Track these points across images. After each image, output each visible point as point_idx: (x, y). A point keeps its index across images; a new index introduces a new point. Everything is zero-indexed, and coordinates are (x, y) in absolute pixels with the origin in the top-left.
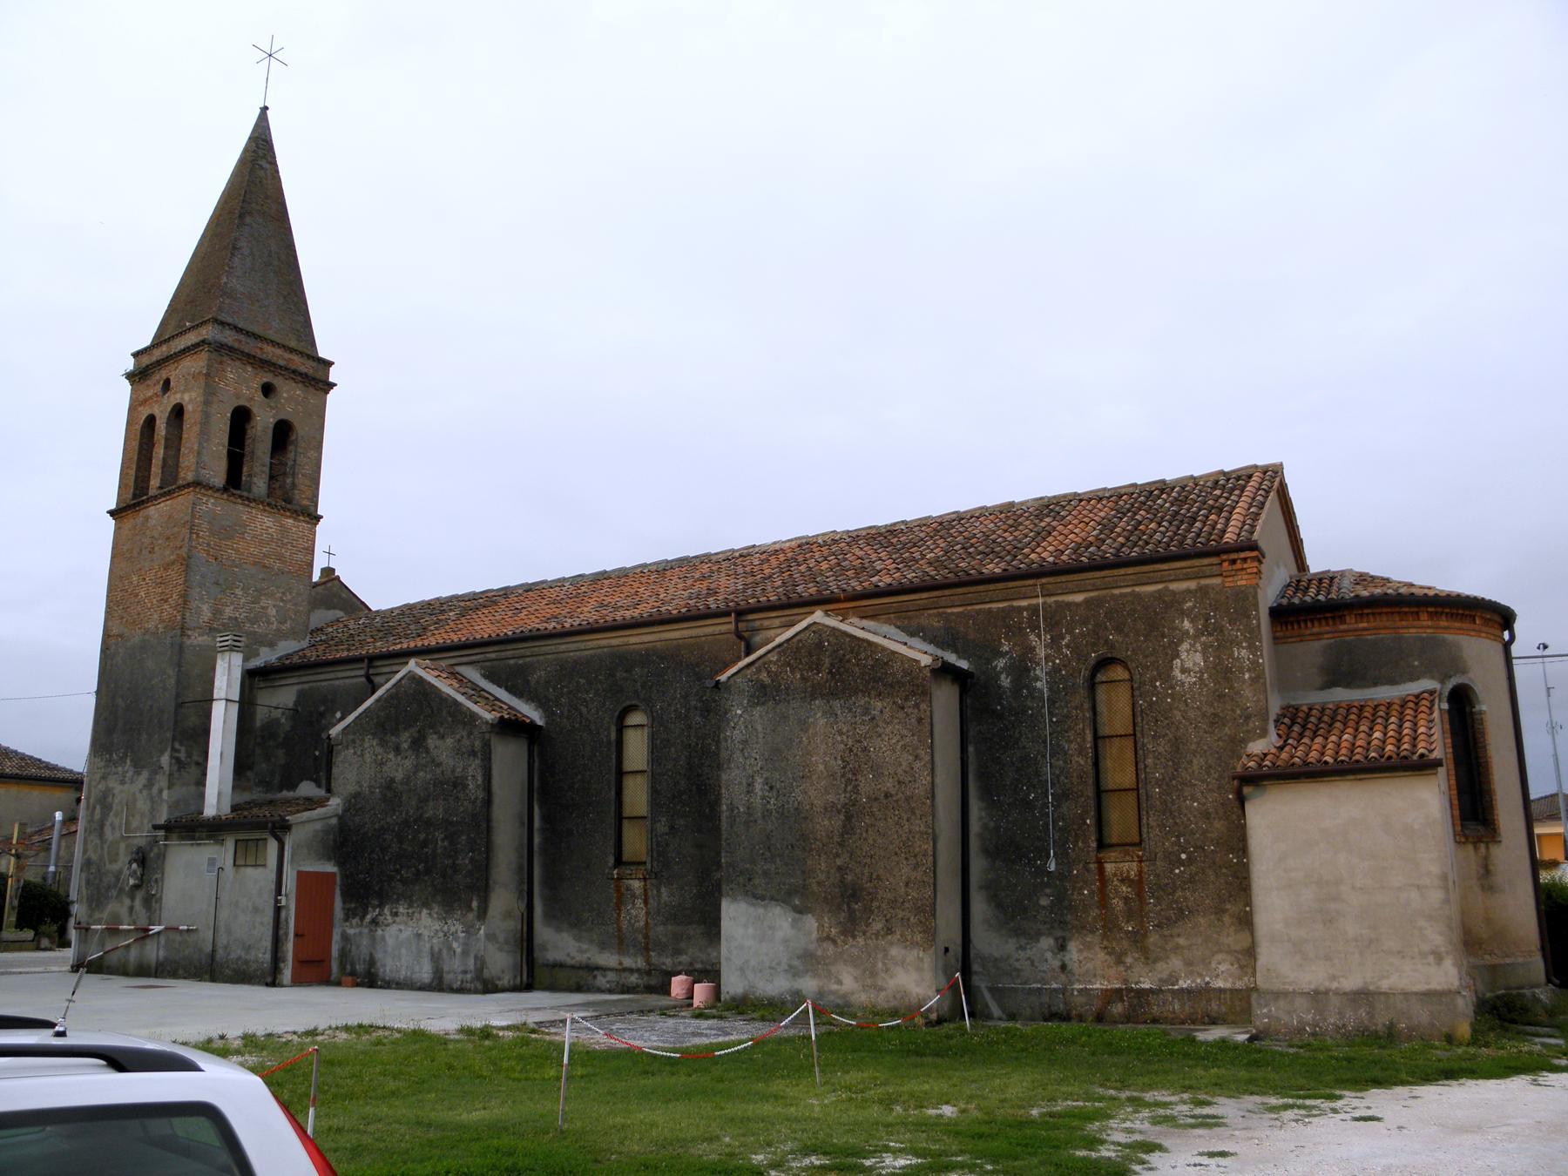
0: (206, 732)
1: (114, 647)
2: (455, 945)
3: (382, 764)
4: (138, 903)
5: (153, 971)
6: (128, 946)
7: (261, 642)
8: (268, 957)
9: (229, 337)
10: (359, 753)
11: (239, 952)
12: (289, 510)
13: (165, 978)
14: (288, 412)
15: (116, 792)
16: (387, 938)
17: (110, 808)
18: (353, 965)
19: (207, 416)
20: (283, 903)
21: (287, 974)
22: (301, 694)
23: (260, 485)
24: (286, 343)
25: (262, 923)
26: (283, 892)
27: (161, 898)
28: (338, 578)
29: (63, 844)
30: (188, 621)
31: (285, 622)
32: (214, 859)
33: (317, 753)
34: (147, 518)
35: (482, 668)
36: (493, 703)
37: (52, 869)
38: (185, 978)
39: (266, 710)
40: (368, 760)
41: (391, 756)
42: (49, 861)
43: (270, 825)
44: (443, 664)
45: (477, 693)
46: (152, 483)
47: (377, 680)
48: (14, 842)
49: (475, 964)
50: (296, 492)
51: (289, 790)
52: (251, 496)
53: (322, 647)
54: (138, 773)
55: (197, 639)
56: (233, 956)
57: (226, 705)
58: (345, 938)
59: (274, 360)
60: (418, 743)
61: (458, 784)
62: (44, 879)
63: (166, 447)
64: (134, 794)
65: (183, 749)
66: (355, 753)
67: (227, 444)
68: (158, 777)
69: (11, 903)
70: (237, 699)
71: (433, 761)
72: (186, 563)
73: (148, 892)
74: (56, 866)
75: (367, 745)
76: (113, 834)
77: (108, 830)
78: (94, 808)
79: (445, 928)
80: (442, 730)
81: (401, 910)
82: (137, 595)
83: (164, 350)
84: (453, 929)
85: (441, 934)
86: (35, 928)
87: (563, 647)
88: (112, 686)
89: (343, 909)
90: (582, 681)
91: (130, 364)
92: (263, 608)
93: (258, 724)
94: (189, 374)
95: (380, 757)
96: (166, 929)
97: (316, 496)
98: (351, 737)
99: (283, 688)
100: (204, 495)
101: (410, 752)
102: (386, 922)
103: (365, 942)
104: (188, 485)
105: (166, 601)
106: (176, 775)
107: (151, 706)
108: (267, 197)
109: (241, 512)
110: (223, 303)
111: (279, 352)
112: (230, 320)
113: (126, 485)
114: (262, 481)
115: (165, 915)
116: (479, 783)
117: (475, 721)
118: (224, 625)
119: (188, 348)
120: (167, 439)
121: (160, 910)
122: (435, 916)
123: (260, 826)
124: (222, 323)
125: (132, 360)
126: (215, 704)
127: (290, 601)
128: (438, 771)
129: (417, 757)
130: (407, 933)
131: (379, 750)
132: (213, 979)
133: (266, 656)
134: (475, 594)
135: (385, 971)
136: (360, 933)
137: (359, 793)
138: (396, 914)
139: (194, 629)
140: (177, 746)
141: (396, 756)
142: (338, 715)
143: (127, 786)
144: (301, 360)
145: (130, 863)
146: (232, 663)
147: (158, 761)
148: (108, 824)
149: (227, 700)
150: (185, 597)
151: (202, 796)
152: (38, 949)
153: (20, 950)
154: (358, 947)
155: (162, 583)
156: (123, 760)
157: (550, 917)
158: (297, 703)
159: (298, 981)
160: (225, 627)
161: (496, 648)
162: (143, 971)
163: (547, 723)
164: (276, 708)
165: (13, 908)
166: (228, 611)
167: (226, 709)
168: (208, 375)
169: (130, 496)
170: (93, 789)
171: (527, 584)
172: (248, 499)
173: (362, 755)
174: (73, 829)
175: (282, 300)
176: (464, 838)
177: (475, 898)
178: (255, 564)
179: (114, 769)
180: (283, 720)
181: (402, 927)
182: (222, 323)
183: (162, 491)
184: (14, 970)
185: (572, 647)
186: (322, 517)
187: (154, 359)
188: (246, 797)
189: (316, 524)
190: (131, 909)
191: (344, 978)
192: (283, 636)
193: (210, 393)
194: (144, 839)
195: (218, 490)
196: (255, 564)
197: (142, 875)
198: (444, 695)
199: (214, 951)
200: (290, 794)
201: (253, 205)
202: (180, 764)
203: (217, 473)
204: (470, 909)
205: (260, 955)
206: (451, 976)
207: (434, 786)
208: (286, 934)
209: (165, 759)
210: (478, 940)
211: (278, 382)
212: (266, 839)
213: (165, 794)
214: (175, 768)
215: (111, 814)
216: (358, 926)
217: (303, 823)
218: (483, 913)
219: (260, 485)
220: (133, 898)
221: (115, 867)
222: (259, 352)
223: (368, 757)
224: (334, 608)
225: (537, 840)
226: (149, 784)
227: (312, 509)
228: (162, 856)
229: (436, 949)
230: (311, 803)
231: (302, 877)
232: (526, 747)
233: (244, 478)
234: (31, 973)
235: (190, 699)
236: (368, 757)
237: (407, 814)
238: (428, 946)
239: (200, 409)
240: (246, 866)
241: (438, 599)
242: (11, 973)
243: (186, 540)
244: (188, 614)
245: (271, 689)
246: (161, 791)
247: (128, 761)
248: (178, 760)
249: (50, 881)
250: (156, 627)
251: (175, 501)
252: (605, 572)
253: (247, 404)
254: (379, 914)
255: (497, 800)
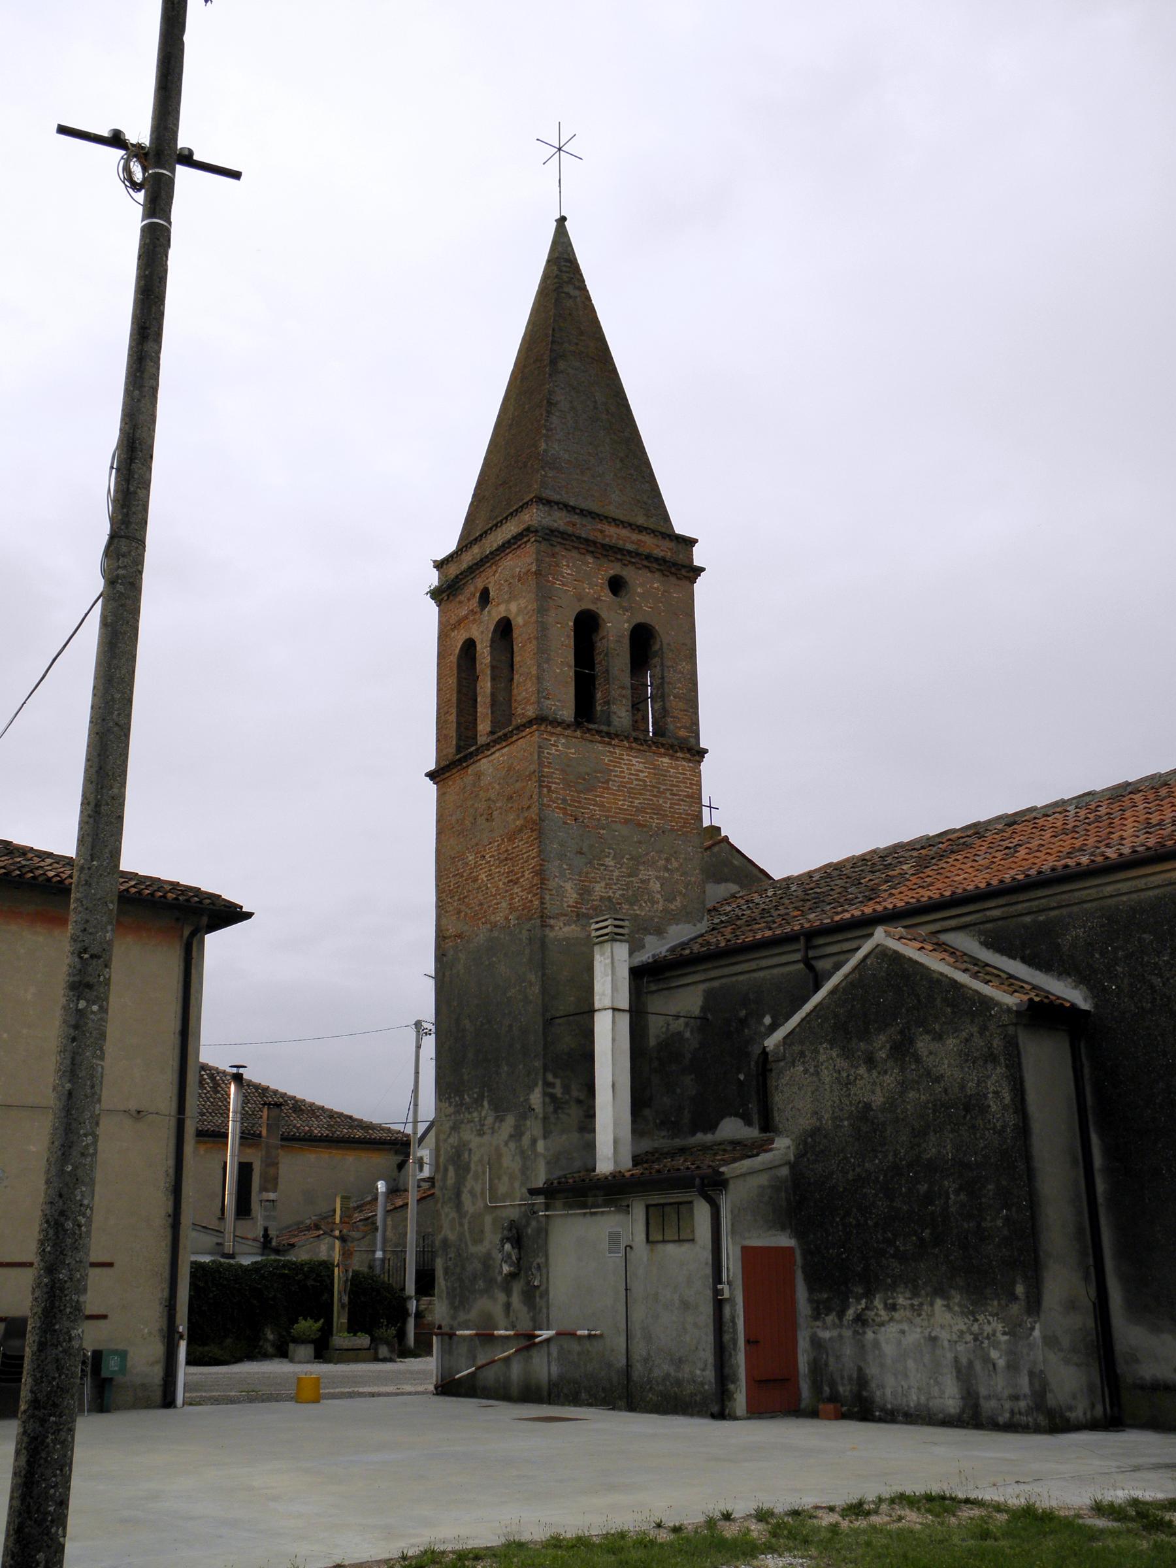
0: (588, 1057)
1: (451, 952)
2: (994, 1354)
3: (848, 1083)
4: (516, 1299)
5: (545, 1394)
6: (507, 1360)
7: (645, 929)
8: (710, 1374)
9: (559, 520)
10: (812, 1070)
11: (666, 1367)
12: (663, 745)
13: (563, 1404)
14: (646, 612)
15: (473, 1145)
16: (883, 1345)
17: (467, 1169)
18: (833, 1385)
19: (543, 628)
20: (726, 1295)
21: (740, 1400)
22: (709, 995)
23: (622, 715)
24: (632, 520)
25: (695, 1325)
26: (725, 1278)
27: (547, 1291)
28: (726, 839)
29: (389, 1222)
30: (548, 905)
31: (674, 899)
32: (618, 1234)
33: (742, 1077)
34: (479, 775)
35: (980, 933)
36: (1010, 982)
37: (379, 1254)
38: (590, 1405)
39: (661, 1021)
40: (827, 1080)
41: (862, 1071)
42: (376, 1247)
43: (697, 1181)
44: (922, 931)
45: (981, 969)
46: (480, 727)
47: (822, 965)
48: (338, 1220)
49: (1031, 1383)
50: (669, 720)
51: (705, 1131)
52: (612, 731)
53: (729, 929)
54: (500, 1119)
55: (563, 930)
56: (657, 1373)
57: (614, 1016)
58: (816, 1343)
59: (620, 544)
60: (902, 1050)
61: (973, 1106)
62: (371, 1267)
63: (493, 679)
64: (497, 1149)
65: (558, 1082)
66: (806, 1071)
67: (572, 662)
68: (528, 1123)
69: (340, 1299)
70: (627, 1007)
71: (929, 1074)
72: (538, 828)
73: (528, 1283)
74: (384, 1251)
75: (822, 1058)
76: (474, 1204)
77: (466, 1198)
78: (446, 1170)
79: (975, 1328)
80: (937, 1027)
81: (901, 1300)
82: (475, 880)
83: (476, 552)
84: (988, 1329)
85: (969, 1338)
86: (369, 1332)
87: (1109, 889)
88: (455, 1004)
89: (810, 1301)
90: (1148, 937)
91: (433, 579)
92: (643, 881)
93: (652, 1042)
94: (513, 577)
95: (844, 1074)
96: (558, 1334)
97: (696, 723)
98: (797, 1048)
99: (680, 990)
100: (552, 734)
101: (890, 1064)
102: (878, 1320)
103: (848, 1350)
104: (530, 723)
105: (516, 883)
106: (552, 1119)
107: (510, 1026)
108: (582, 333)
109: (601, 753)
110: (545, 476)
111: (625, 532)
112: (556, 497)
113: (446, 736)
114: (624, 709)
115: (554, 1314)
116: (1007, 1100)
117: (989, 1009)
118: (595, 908)
119: (509, 542)
120: (493, 668)
121: (548, 1308)
122: (956, 1308)
123: (681, 1182)
124: (548, 503)
125: (435, 573)
126: (598, 1017)
127: (677, 870)
128: (938, 1088)
129: (903, 1070)
130: (914, 1336)
131: (841, 1063)
132: (632, 1407)
133: (655, 948)
134: (928, 838)
135: (884, 1394)
136: (840, 1336)
137: (818, 1129)
138: (893, 1308)
139: (556, 917)
140: (550, 1078)
141: (869, 1071)
142: (767, 1020)
143: (486, 1138)
144: (655, 541)
145: (503, 1242)
146: (616, 958)
147: (527, 1100)
148: (465, 1190)
149: (614, 1009)
150: (541, 874)
151: (591, 1146)
152: (377, 1359)
153: (356, 1360)
154: (838, 1358)
155: (508, 858)
156: (478, 1101)
157: (1138, 1309)
158: (704, 1009)
159: (757, 1411)
160: (597, 911)
161: (1001, 901)
162: (529, 1394)
163: (1096, 1006)
164: (678, 1017)
165: (343, 1306)
166: (599, 889)
167: (614, 1022)
168: (538, 574)
169: (453, 750)
170: (441, 1144)
171: (1007, 816)
172: (608, 734)
173: (817, 1073)
174: (399, 1202)
175: (619, 465)
176: (990, 1187)
177: (1019, 1279)
178: (627, 821)
179: (467, 1115)
180: (688, 1035)
181: (905, 1327)
182: (548, 503)
183: (496, 736)
184: (361, 1390)
185: (1124, 887)
186: (706, 751)
187: (464, 566)
188: (646, 1145)
189: (700, 762)
190: (508, 1306)
191: (821, 1406)
192: (673, 917)
193: (544, 596)
194: (517, 1209)
195: (568, 726)
196: (627, 821)
197: (519, 1259)
198: (935, 976)
199: (629, 1365)
200: (709, 1138)
201: (566, 345)
202: (555, 1103)
203: (564, 706)
204: (1014, 1297)
205: (698, 1372)
206: (993, 1403)
207: (934, 1111)
208: (735, 1341)
209: (536, 1098)
210: (1031, 1347)
211: (628, 573)
212: (691, 1202)
213: (540, 1146)
214: (551, 1109)
215: (469, 1176)
216: (834, 1326)
217: (743, 1175)
218: (1034, 1305)
219: (622, 715)
220: (508, 1293)
221: (481, 1249)
222: (599, 536)
223: (826, 1076)
224: (726, 881)
225: (1101, 1187)
226: (517, 1134)
227: (692, 740)
228: (543, 1232)
229: (964, 1361)
230: (744, 1149)
231: (748, 1253)
232: (1067, 1045)
233: (599, 708)
234: (379, 1395)
235: (562, 1013)
236: (826, 1076)
237: (895, 1155)
238: (950, 1356)
239: (533, 619)
240: (664, 1241)
241: (874, 851)
242: (361, 1395)
243: (535, 797)
244: (547, 897)
245: (666, 992)
246: (534, 1142)
247: (486, 1103)
248: (553, 1097)
249: (378, 1271)
250: (506, 918)
251: (513, 747)
252: (1128, 784)
253: (592, 607)
254: (867, 1308)
255: (1036, 1127)
